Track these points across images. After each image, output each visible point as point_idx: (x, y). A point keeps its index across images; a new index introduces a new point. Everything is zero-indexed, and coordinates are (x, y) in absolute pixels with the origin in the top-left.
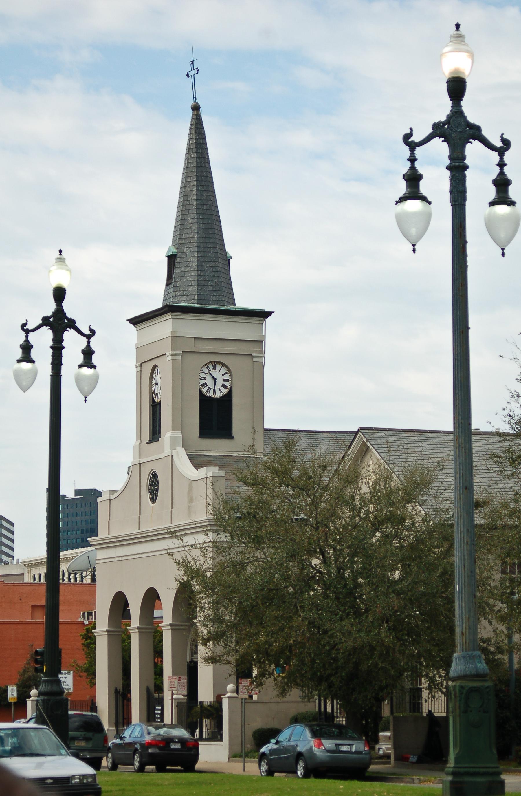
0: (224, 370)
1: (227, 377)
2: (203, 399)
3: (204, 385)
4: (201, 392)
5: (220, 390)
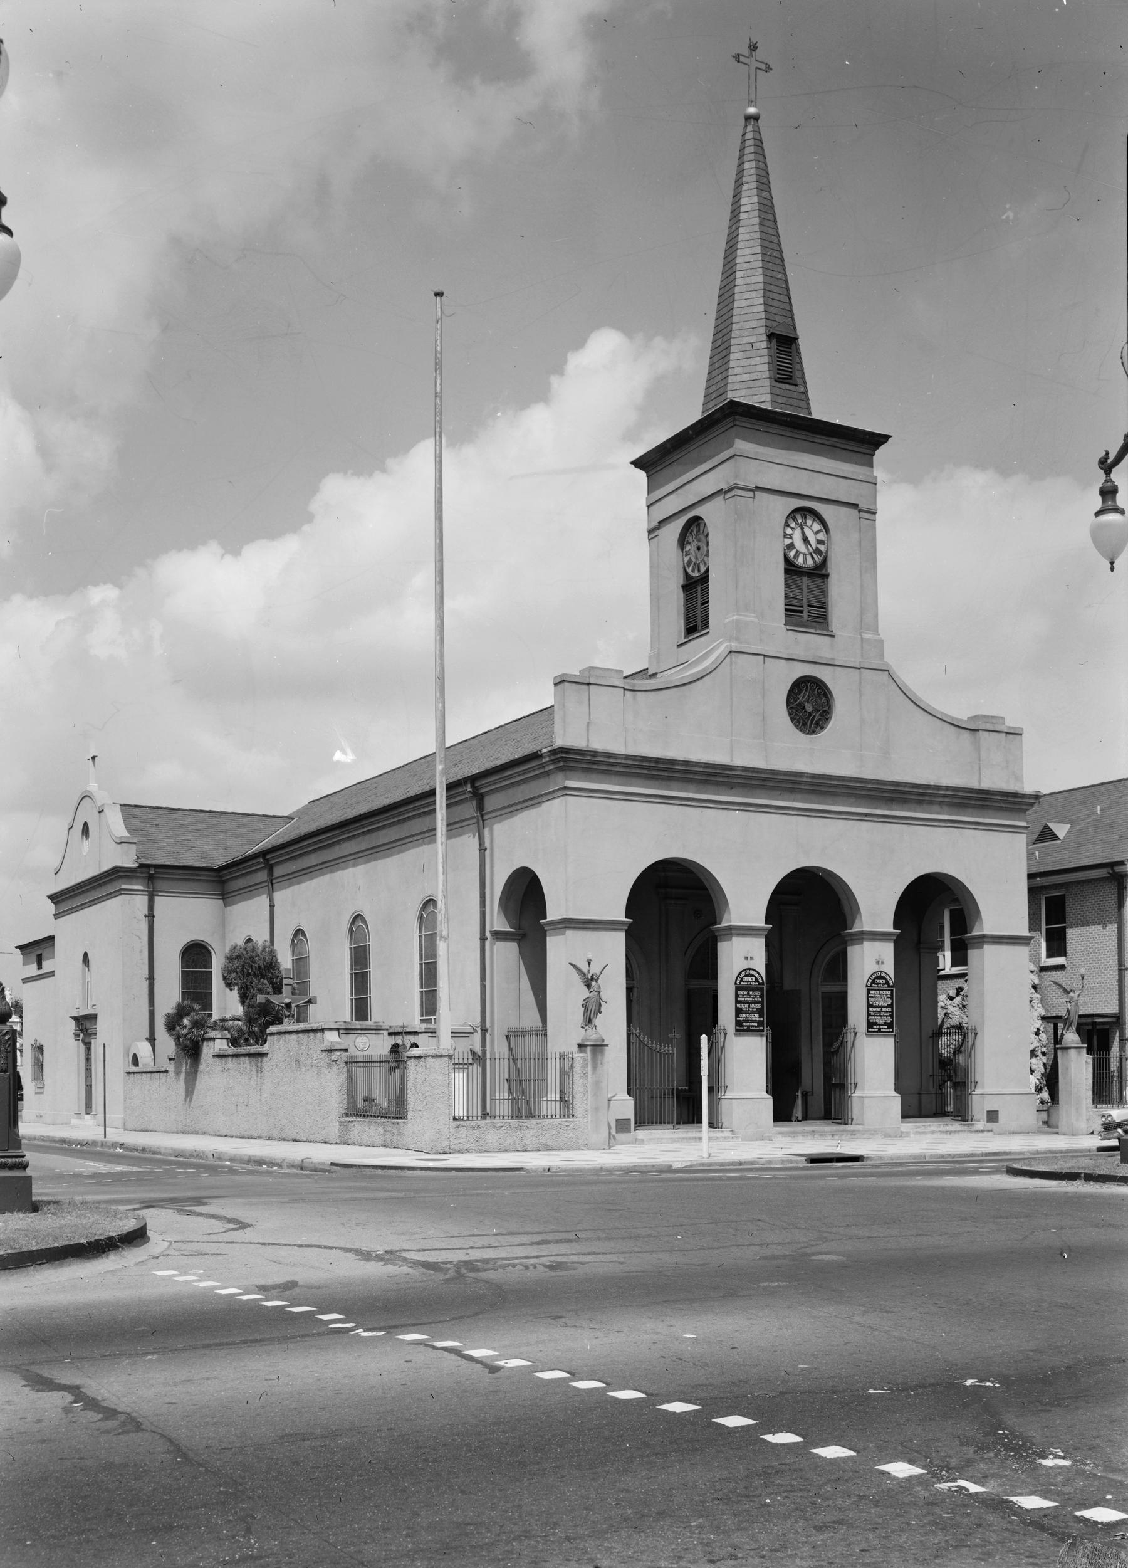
0: (817, 526)
1: (821, 536)
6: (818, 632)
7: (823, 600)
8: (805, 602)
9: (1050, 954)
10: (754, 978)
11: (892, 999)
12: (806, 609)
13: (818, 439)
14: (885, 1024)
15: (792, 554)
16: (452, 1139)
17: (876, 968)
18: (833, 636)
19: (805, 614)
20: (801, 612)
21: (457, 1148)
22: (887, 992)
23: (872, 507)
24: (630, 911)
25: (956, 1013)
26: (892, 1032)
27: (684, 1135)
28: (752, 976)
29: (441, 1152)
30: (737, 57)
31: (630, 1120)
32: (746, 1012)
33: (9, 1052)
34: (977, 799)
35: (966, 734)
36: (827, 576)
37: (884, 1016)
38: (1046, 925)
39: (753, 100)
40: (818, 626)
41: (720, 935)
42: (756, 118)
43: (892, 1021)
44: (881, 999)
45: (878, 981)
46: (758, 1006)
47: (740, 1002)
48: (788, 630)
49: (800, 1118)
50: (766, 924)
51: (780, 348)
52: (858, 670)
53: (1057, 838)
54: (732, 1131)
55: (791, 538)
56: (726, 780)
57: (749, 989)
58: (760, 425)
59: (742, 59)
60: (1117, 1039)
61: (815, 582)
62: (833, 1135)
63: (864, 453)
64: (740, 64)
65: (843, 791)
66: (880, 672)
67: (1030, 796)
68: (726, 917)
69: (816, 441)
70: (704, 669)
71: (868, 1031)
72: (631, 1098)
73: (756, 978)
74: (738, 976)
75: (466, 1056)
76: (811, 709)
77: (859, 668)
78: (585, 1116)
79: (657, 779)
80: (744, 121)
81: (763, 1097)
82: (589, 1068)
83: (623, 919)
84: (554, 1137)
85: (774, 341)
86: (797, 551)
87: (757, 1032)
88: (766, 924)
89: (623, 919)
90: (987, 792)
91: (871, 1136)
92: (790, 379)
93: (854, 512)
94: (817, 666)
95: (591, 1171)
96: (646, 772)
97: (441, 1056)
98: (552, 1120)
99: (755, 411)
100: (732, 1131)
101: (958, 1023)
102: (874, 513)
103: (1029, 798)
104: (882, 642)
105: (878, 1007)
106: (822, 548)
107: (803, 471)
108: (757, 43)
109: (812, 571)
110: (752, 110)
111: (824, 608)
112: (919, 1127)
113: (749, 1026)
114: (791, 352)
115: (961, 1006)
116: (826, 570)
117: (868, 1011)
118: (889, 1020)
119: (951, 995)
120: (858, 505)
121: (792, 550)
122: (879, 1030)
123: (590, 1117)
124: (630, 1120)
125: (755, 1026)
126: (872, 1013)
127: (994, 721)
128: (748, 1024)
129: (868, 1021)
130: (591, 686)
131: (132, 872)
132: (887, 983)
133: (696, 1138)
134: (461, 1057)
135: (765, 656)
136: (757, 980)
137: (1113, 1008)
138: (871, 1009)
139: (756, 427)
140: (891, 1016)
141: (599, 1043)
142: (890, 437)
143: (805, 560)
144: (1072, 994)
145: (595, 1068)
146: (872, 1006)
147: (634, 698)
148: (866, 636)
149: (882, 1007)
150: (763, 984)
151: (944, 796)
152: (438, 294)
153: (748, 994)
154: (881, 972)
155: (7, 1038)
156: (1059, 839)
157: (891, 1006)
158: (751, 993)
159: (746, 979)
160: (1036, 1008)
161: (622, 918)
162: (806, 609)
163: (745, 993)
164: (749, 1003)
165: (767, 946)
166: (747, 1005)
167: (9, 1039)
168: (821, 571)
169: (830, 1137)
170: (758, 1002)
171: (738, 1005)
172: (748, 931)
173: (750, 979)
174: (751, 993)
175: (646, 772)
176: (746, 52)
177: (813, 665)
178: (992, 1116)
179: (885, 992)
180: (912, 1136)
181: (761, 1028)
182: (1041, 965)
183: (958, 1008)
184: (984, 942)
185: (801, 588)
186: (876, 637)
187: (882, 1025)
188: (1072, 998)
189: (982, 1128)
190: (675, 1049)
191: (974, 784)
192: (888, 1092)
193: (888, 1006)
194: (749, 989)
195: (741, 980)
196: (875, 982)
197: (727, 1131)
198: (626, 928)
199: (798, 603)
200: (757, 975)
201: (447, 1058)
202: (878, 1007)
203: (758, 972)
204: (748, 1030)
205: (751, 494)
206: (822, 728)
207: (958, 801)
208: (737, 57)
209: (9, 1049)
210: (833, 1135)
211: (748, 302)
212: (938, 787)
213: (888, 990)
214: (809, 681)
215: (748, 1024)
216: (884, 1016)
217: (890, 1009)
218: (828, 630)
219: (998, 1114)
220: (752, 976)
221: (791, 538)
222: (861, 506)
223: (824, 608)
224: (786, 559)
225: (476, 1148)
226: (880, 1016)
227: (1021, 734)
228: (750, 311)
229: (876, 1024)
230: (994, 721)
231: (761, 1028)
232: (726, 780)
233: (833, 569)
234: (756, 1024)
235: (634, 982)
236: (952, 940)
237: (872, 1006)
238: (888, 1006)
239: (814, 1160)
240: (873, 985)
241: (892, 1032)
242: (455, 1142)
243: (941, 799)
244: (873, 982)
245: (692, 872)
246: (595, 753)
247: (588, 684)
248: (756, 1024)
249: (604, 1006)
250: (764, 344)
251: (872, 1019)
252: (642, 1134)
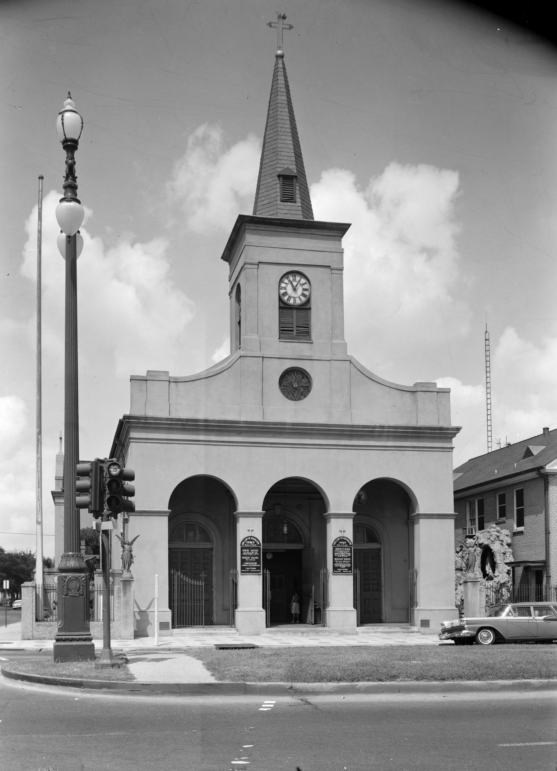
0: (303, 281)
1: (306, 286)
3: (285, 294)
5: (300, 298)
6: (301, 341)
7: (307, 323)
8: (295, 325)
9: (518, 526)
10: (254, 542)
11: (351, 553)
12: (295, 329)
13: (302, 231)
14: (346, 568)
15: (286, 298)
16: (34, 632)
17: (340, 535)
18: (312, 343)
19: (295, 332)
20: (292, 331)
21: (37, 637)
22: (348, 549)
23: (340, 267)
24: (171, 505)
25: (459, 561)
26: (352, 572)
27: (204, 632)
28: (252, 540)
29: (27, 639)
30: (270, 25)
31: (169, 623)
32: (248, 561)
33: (84, 586)
34: (413, 433)
35: (408, 394)
36: (310, 309)
37: (345, 563)
38: (517, 507)
39: (281, 46)
40: (303, 338)
41: (328, 519)
42: (282, 56)
43: (351, 566)
44: (342, 553)
45: (341, 542)
46: (257, 558)
47: (244, 556)
48: (280, 341)
49: (313, 623)
50: (169, 509)
51: (285, 183)
52: (329, 362)
53: (532, 455)
54: (237, 630)
55: (285, 289)
56: (235, 429)
57: (250, 548)
58: (262, 227)
59: (273, 25)
60: (545, 575)
61: (301, 313)
62: (303, 633)
63: (335, 236)
64: (272, 28)
65: (316, 432)
66: (344, 362)
67: (453, 429)
68: (417, 510)
69: (301, 232)
70: (223, 368)
71: (334, 572)
72: (171, 610)
73: (255, 542)
74: (243, 541)
75: (99, 587)
76: (297, 386)
77: (330, 361)
78: (119, 620)
79: (190, 431)
80: (275, 58)
81: (260, 610)
82: (122, 594)
83: (351, 512)
84: (99, 632)
85: (281, 179)
86: (289, 296)
87: (256, 572)
88: (169, 509)
89: (351, 512)
90: (420, 428)
91: (330, 634)
92: (293, 199)
93: (329, 270)
94: (301, 361)
95: (272, 649)
96: (181, 427)
97: (27, 587)
98: (98, 622)
99: (256, 219)
100: (237, 630)
101: (460, 567)
102: (342, 270)
103: (452, 430)
104: (346, 343)
105: (341, 557)
106: (307, 293)
107: (292, 250)
108: (285, 15)
109: (299, 307)
110: (279, 52)
111: (308, 327)
112: (370, 629)
113: (251, 570)
114: (293, 184)
115: (462, 557)
116: (310, 305)
117: (334, 560)
118: (349, 565)
119: (457, 550)
120: (330, 266)
121: (286, 296)
122: (342, 571)
123: (121, 621)
124: (169, 623)
125: (255, 570)
126: (337, 562)
127: (427, 385)
128: (249, 568)
129: (334, 566)
130: (148, 381)
131: (60, 494)
132: (347, 543)
133: (207, 634)
134: (99, 587)
135: (263, 357)
136: (256, 543)
137: (543, 558)
138: (336, 559)
139: (260, 229)
140: (351, 563)
141: (127, 579)
142: (349, 225)
143: (295, 300)
144: (470, 549)
145: (125, 593)
146: (337, 557)
147: (177, 386)
148: (334, 341)
149: (344, 557)
150: (260, 545)
151: (388, 432)
152: (41, 178)
153: (250, 551)
154: (343, 537)
155: (83, 579)
156: (534, 455)
157: (350, 557)
158: (251, 551)
159: (248, 542)
160: (508, 557)
161: (166, 509)
162: (295, 329)
163: (248, 550)
164: (250, 557)
165: (169, 521)
166: (249, 558)
167: (84, 580)
168: (306, 306)
169: (301, 634)
170: (257, 556)
171: (243, 558)
173: (251, 542)
174: (251, 551)
175: (181, 427)
176: (275, 20)
177: (297, 361)
178: (425, 623)
179: (346, 549)
180: (360, 634)
181: (259, 570)
182: (514, 532)
183: (460, 558)
184: (419, 518)
185: (292, 317)
186: (342, 342)
187: (344, 568)
188: (470, 551)
189: (417, 630)
190: (203, 583)
191: (413, 424)
192: (350, 608)
193: (348, 557)
194: (250, 548)
195: (245, 543)
196: (340, 542)
197: (233, 630)
198: (353, 517)
199: (290, 326)
200: (256, 540)
201: (31, 588)
202: (341, 557)
203: (256, 539)
204: (250, 572)
205: (256, 266)
206: (305, 396)
207: (400, 434)
208: (270, 25)
209: (84, 585)
210: (303, 633)
211: (270, 160)
212: (382, 427)
213: (349, 548)
214: (295, 370)
215: (249, 568)
216: (345, 563)
217: (349, 559)
218: (310, 340)
219: (429, 622)
220: (252, 540)
221: (285, 289)
222: (333, 266)
223: (308, 327)
224: (280, 300)
225: (50, 637)
226: (342, 563)
227: (449, 392)
228: (271, 164)
229: (339, 568)
230: (427, 385)
231: (259, 570)
232: (235, 429)
233: (313, 305)
234: (255, 569)
235: (214, 545)
236: (479, 518)
237: (337, 557)
238: (348, 557)
239: (222, 648)
240: (338, 545)
241: (352, 572)
242: (36, 633)
243: (387, 434)
244: (337, 543)
245: (311, 484)
246: (146, 418)
247: (146, 380)
248: (255, 569)
249: (135, 560)
250: (278, 182)
251: (336, 565)
252: (176, 631)
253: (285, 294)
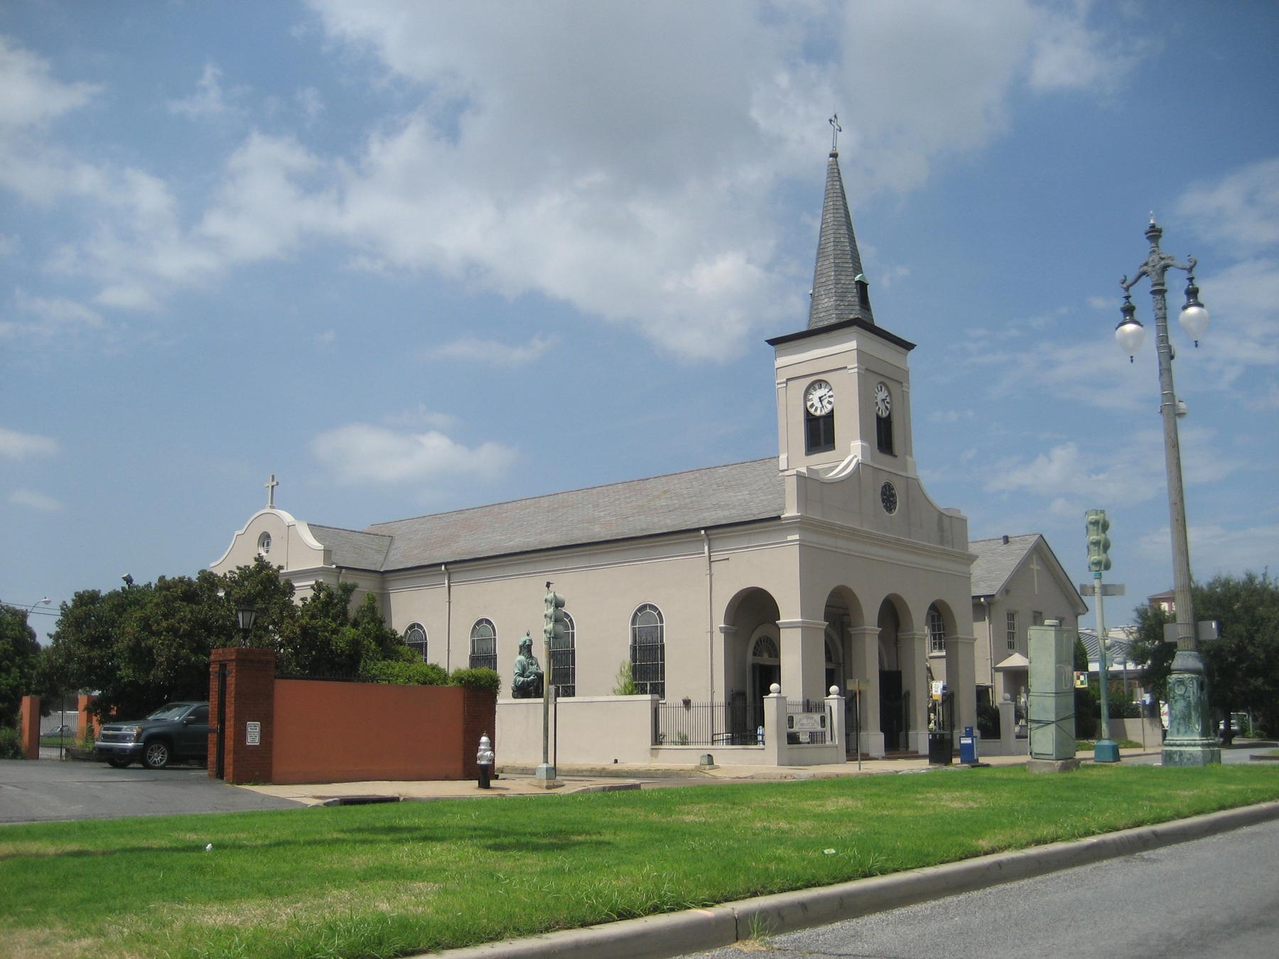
2: (879, 418)
4: (877, 415)
172: (791, 626)
224: (877, 415)
253: (812, 406)
